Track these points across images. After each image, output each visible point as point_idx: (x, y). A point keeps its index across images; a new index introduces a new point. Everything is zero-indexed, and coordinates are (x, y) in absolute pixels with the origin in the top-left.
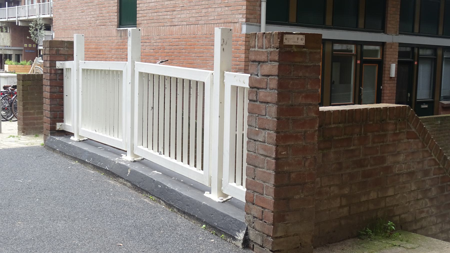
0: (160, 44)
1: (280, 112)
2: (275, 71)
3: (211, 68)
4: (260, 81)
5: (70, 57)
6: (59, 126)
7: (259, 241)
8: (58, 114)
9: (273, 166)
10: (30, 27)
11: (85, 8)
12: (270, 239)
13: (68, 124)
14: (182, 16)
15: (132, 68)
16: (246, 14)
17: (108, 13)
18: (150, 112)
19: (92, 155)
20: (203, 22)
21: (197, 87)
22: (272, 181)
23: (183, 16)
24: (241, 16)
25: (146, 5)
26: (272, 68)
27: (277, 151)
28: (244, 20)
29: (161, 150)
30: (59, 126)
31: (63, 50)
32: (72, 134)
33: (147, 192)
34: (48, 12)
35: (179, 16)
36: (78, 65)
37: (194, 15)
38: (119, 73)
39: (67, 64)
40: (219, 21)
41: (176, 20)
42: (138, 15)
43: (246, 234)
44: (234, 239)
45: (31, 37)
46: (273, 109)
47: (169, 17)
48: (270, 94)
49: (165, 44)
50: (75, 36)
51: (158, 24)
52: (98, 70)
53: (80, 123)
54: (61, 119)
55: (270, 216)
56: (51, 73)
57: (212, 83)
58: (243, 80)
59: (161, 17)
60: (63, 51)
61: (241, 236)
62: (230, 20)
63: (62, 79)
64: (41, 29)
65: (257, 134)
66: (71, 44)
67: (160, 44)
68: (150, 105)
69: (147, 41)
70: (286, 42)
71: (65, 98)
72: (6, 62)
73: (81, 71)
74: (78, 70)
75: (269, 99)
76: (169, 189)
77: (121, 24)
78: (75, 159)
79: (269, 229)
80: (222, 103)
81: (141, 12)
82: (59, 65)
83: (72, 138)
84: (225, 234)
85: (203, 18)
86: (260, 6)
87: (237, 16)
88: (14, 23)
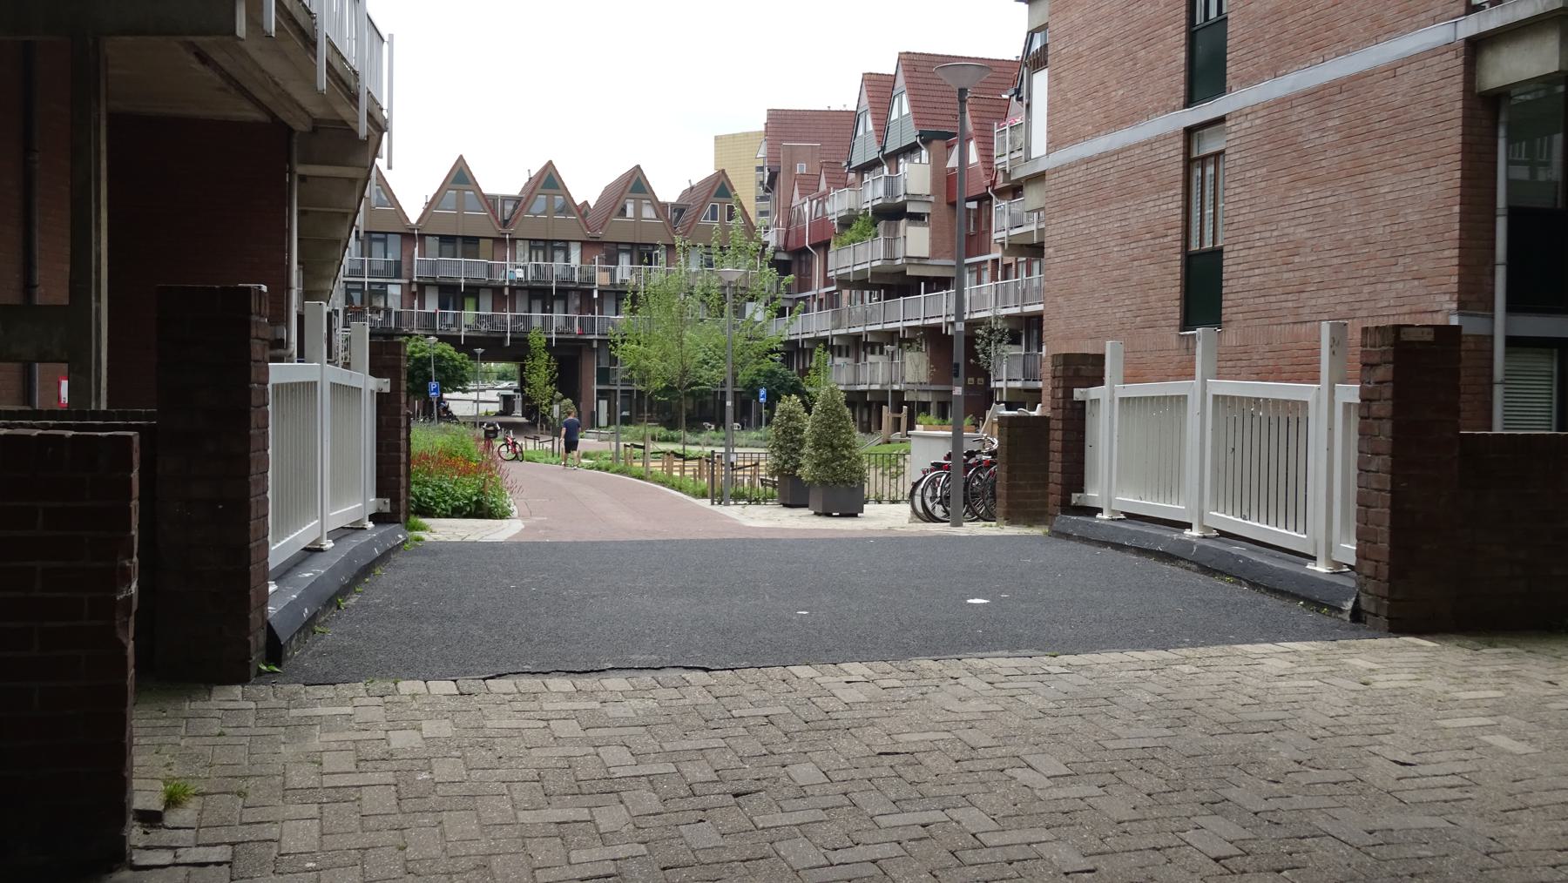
0: (1271, 362)
1: (1396, 429)
2: (1389, 376)
3: (1316, 380)
4: (1372, 391)
5: (1099, 381)
6: (1075, 498)
7: (1372, 610)
8: (1075, 478)
9: (1388, 503)
10: (977, 336)
11: (1112, 292)
12: (1386, 602)
13: (1093, 494)
14: (1321, 301)
15: (1201, 390)
16: (1459, 292)
17: (1161, 300)
18: (1230, 456)
19: (1134, 534)
20: (1364, 313)
21: (1297, 409)
22: (1387, 523)
23: (1321, 301)
24: (1447, 297)
25: (1242, 281)
26: (1384, 372)
27: (1393, 482)
28: (1455, 306)
29: (1245, 513)
30: (1075, 498)
31: (1085, 369)
32: (1100, 510)
33: (1222, 573)
34: (1016, 300)
35: (1313, 302)
36: (1113, 391)
37: (1344, 299)
38: (1181, 400)
39: (1094, 392)
40: (1399, 310)
41: (1306, 310)
42: (1224, 304)
43: (1357, 602)
44: (1341, 611)
45: (978, 359)
46: (1387, 426)
47: (1290, 304)
48: (1383, 408)
49: (1281, 362)
50: (1108, 343)
51: (1267, 321)
52: (1146, 398)
53: (1112, 489)
54: (1080, 488)
55: (1385, 570)
56: (1064, 408)
57: (1318, 402)
58: (1350, 393)
59: (1275, 306)
60: (1086, 370)
61: (1349, 605)
62: (1423, 306)
63: (1084, 420)
64: (1000, 341)
65: (1369, 462)
66: (1099, 359)
67: (1271, 362)
68: (1230, 446)
69: (1244, 356)
70: (1404, 337)
71: (1088, 450)
72: (919, 419)
73: (1117, 401)
74: (1112, 401)
75: (1382, 413)
76: (1254, 563)
77: (1188, 322)
78: (1105, 544)
79: (1384, 588)
80: (1331, 429)
81: (1231, 296)
82: (1078, 394)
83: (1099, 516)
84: (1329, 607)
85: (1365, 305)
86: (1493, 274)
87: (1438, 298)
88: (937, 328)
